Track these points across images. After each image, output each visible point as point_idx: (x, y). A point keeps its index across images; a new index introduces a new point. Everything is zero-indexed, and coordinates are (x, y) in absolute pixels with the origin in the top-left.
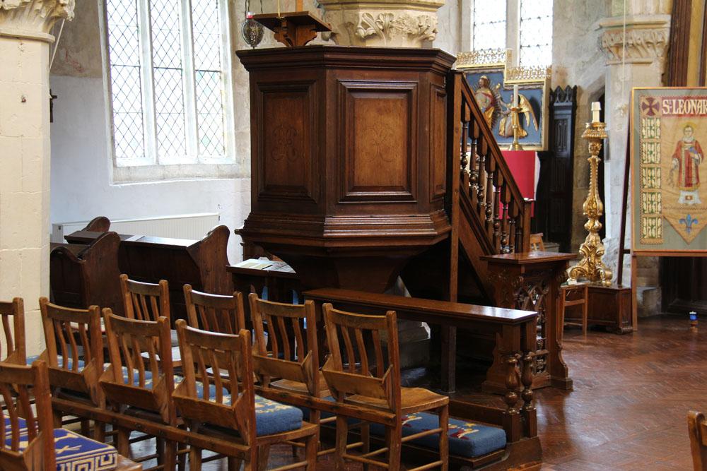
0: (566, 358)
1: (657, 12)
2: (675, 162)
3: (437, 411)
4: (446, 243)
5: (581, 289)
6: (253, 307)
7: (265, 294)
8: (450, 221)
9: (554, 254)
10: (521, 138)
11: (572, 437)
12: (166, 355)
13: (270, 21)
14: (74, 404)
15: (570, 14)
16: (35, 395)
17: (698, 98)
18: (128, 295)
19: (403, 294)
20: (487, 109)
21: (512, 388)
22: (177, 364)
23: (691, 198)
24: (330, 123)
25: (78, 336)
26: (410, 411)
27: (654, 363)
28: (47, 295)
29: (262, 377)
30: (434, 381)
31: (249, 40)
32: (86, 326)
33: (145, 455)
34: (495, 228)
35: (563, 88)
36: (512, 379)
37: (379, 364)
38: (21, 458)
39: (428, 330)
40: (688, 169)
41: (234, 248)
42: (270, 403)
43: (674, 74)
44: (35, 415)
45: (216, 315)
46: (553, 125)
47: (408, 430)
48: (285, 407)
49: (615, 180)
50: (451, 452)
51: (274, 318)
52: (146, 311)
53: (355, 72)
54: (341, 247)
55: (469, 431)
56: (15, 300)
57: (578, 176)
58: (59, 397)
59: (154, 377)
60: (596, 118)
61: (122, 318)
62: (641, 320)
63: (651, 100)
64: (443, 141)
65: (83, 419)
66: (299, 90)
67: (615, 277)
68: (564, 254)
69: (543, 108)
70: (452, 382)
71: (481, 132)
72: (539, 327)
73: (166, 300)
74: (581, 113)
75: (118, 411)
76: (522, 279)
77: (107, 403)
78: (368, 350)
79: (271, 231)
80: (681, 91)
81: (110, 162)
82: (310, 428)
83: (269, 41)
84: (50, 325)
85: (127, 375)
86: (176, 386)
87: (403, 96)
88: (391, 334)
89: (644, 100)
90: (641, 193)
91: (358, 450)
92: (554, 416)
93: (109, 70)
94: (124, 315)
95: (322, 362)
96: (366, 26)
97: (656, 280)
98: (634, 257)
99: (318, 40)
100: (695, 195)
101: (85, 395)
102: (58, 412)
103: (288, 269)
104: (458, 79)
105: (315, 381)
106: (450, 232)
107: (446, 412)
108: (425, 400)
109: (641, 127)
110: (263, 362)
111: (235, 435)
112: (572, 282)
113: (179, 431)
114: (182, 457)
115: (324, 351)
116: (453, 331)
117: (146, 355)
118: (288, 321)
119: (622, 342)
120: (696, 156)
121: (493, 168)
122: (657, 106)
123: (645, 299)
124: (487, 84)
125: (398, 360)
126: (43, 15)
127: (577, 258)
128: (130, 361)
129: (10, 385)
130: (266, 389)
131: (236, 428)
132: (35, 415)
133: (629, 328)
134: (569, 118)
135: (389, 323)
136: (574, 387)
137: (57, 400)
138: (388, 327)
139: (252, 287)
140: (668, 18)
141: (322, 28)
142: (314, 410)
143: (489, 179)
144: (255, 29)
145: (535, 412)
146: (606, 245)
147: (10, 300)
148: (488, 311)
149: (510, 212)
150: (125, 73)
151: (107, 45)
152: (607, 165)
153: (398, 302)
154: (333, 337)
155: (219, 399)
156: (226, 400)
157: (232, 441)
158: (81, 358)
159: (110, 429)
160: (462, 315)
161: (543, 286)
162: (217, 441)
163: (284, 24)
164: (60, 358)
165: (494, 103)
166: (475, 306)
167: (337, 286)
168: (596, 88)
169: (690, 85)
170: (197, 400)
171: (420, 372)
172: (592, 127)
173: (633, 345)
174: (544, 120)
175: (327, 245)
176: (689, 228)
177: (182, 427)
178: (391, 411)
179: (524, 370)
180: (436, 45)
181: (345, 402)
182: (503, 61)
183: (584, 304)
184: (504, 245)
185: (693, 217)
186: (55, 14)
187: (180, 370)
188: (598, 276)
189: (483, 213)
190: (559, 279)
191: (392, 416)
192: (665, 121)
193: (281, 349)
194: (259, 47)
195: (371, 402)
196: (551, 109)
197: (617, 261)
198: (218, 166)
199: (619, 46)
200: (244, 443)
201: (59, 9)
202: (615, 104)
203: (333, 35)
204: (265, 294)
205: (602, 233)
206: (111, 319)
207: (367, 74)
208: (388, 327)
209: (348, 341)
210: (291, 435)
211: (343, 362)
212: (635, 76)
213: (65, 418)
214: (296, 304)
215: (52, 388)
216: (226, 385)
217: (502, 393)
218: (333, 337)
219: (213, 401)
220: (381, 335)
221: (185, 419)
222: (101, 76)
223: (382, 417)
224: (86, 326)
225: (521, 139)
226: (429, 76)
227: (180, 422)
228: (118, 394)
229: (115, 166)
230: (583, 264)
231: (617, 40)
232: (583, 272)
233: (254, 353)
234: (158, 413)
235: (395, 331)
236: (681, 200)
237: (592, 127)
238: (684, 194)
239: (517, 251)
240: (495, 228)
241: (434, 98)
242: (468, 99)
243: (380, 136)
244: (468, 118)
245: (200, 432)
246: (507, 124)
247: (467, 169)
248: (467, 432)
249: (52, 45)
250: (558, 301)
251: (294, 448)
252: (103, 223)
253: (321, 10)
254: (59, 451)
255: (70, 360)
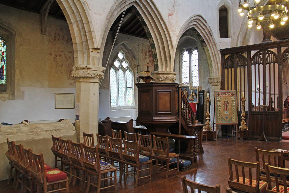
0: (203, 146)
1: (219, 76)
2: (224, 105)
3: (177, 157)
4: (178, 123)
5: (206, 132)
6: (138, 136)
7: (141, 133)
8: (179, 118)
9: (200, 125)
10: (193, 100)
11: (204, 162)
12: (121, 146)
13: (142, 78)
14: (103, 155)
15: (202, 76)
16: (95, 153)
17: (227, 93)
18: (113, 133)
19: (169, 133)
20: (186, 95)
21: (192, 153)
22: (123, 147)
23: (227, 113)
24: (154, 98)
25: (104, 141)
26: (171, 158)
27: (220, 147)
28: (98, 133)
29: (140, 150)
30: (176, 151)
31: (138, 82)
32: (105, 139)
33: (117, 166)
34: (188, 119)
35: (201, 90)
36: (192, 151)
37: (165, 148)
38: (93, 165)
39: (175, 141)
40: (226, 107)
41: (134, 123)
42: (142, 156)
43: (222, 88)
44: (96, 157)
45: (131, 138)
46: (199, 98)
47: (171, 161)
48: (145, 157)
49: (212, 109)
50: (179, 166)
51: (143, 139)
52: (117, 136)
53: (159, 88)
54: (225, 74)
55: (183, 161)
56: (92, 134)
57: (205, 108)
58: (100, 153)
59: (118, 150)
60: (208, 97)
61: (112, 138)
62: (218, 138)
63: (219, 93)
64: (177, 101)
65: (105, 158)
66: (148, 91)
67: (213, 129)
68: (202, 125)
69: (197, 95)
70: (180, 152)
71: (185, 100)
72: (197, 140)
73: (121, 134)
74: (205, 96)
75: (111, 157)
76: (194, 130)
77: (110, 155)
78: (163, 145)
79: (142, 120)
80: (224, 91)
81: (110, 106)
82: (151, 161)
83: (142, 81)
84: (98, 139)
85: (113, 150)
86: (123, 152)
87: (169, 92)
88: (167, 142)
89: (217, 93)
90: (217, 112)
91: (160, 166)
92: (200, 158)
93: (110, 88)
94: (112, 137)
95: (153, 147)
96: (161, 78)
97: (220, 130)
98: (216, 125)
99: (152, 81)
100: (228, 112)
101: (105, 153)
102: (100, 157)
103: (146, 128)
104: (180, 89)
105: (151, 151)
106: (179, 120)
107: (179, 158)
108: (174, 155)
109: (217, 98)
110: (140, 147)
111: (135, 162)
112: (204, 130)
113: (123, 161)
114: (124, 166)
115: (153, 145)
116: (180, 141)
117: (117, 145)
118: (146, 139)
119: (214, 142)
120: (228, 104)
121: (188, 107)
122: (220, 94)
123: (218, 134)
124: (186, 90)
125: (168, 146)
126: (98, 78)
127: (205, 125)
128: (114, 147)
129: (91, 151)
130: (141, 153)
131: (135, 161)
132: (96, 157)
133: (215, 140)
134: (203, 96)
135: (167, 140)
136: (205, 152)
137: (100, 154)
138: (166, 140)
139: (138, 132)
140: (221, 77)
141: (152, 79)
142: (151, 157)
143: (187, 109)
144: (139, 79)
145: (197, 157)
146: (211, 122)
147: (91, 134)
148: (187, 137)
149: (191, 116)
150: (113, 88)
151: (110, 83)
152: (210, 106)
153: (168, 135)
154: (155, 142)
155: (132, 155)
156: (133, 155)
157: (134, 163)
158: (104, 146)
159: (110, 160)
160: (182, 137)
161: (198, 131)
162: (132, 164)
163: (145, 78)
164: (100, 146)
165: (187, 93)
166: (184, 136)
167: (156, 132)
168: (208, 90)
169: (226, 90)
170: (127, 155)
171: (173, 149)
172: (207, 98)
173: (216, 143)
174: (197, 97)
175: (154, 123)
176: (227, 119)
177: (124, 160)
178: (168, 158)
179: (195, 149)
180: (175, 82)
181: (158, 156)
182: (189, 85)
183: (206, 135)
184: (190, 123)
185: (227, 117)
186: (101, 78)
187: (124, 149)
188: (209, 129)
189: (186, 116)
190: (201, 129)
191: (167, 159)
192: (221, 97)
193: (144, 145)
194: (140, 83)
195: (163, 156)
196: (199, 95)
197: (213, 126)
198: (131, 107)
199: (212, 82)
200: (137, 164)
201: (101, 77)
202: (212, 93)
203: (155, 80)
204: (141, 133)
205: (210, 120)
206: (110, 138)
207: (162, 88)
208: (166, 140)
209: (158, 143)
210: (146, 163)
211: (157, 147)
212: (215, 88)
213: (101, 158)
214: (147, 135)
215: (99, 152)
216: (133, 152)
217: (190, 154)
218: (155, 142)
219: (130, 155)
220: (165, 142)
221: (125, 159)
222: (108, 89)
223: (165, 159)
224: (105, 139)
225: (193, 101)
226: (174, 88)
227: (124, 159)
228: (112, 153)
229: (111, 107)
230: (206, 127)
231: (211, 81)
232: (206, 128)
233: (139, 145)
234: (119, 158)
235: (168, 141)
236: (225, 113)
237: (207, 98)
238: (226, 112)
239: (193, 124)
240: (188, 119)
241: (175, 92)
242: (182, 93)
243: (164, 101)
244: (182, 97)
245: (128, 161)
246: (190, 98)
247: (182, 107)
248: (183, 162)
249: (100, 83)
250: (201, 134)
251: (147, 165)
252: (108, 118)
253: (152, 75)
254: (101, 164)
255: (102, 146)
